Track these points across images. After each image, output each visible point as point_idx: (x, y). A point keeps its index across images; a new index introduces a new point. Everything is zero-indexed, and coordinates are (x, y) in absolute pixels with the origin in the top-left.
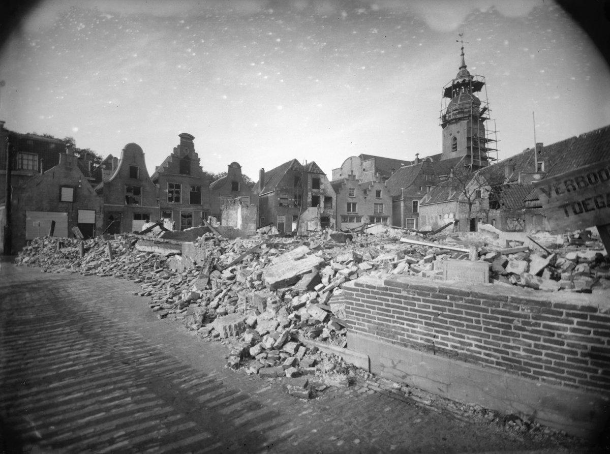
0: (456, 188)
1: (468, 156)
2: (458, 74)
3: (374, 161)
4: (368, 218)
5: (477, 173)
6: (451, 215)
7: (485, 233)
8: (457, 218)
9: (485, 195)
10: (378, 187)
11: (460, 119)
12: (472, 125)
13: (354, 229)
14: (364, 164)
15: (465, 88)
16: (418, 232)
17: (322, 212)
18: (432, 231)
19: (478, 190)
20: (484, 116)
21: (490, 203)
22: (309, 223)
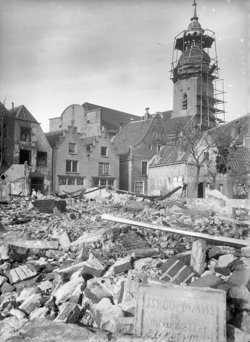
0: (185, 149)
1: (198, 116)
2: (190, 25)
3: (100, 111)
4: (91, 179)
5: (205, 134)
6: (180, 179)
7: (212, 200)
8: (186, 182)
9: (213, 157)
10: (103, 143)
11: (191, 75)
12: (202, 83)
13: (74, 193)
14: (88, 114)
15: (196, 41)
16: (145, 197)
17: (33, 171)
18: (161, 196)
19: (205, 151)
20: (213, 74)
21: (218, 167)
22: (13, 184)
